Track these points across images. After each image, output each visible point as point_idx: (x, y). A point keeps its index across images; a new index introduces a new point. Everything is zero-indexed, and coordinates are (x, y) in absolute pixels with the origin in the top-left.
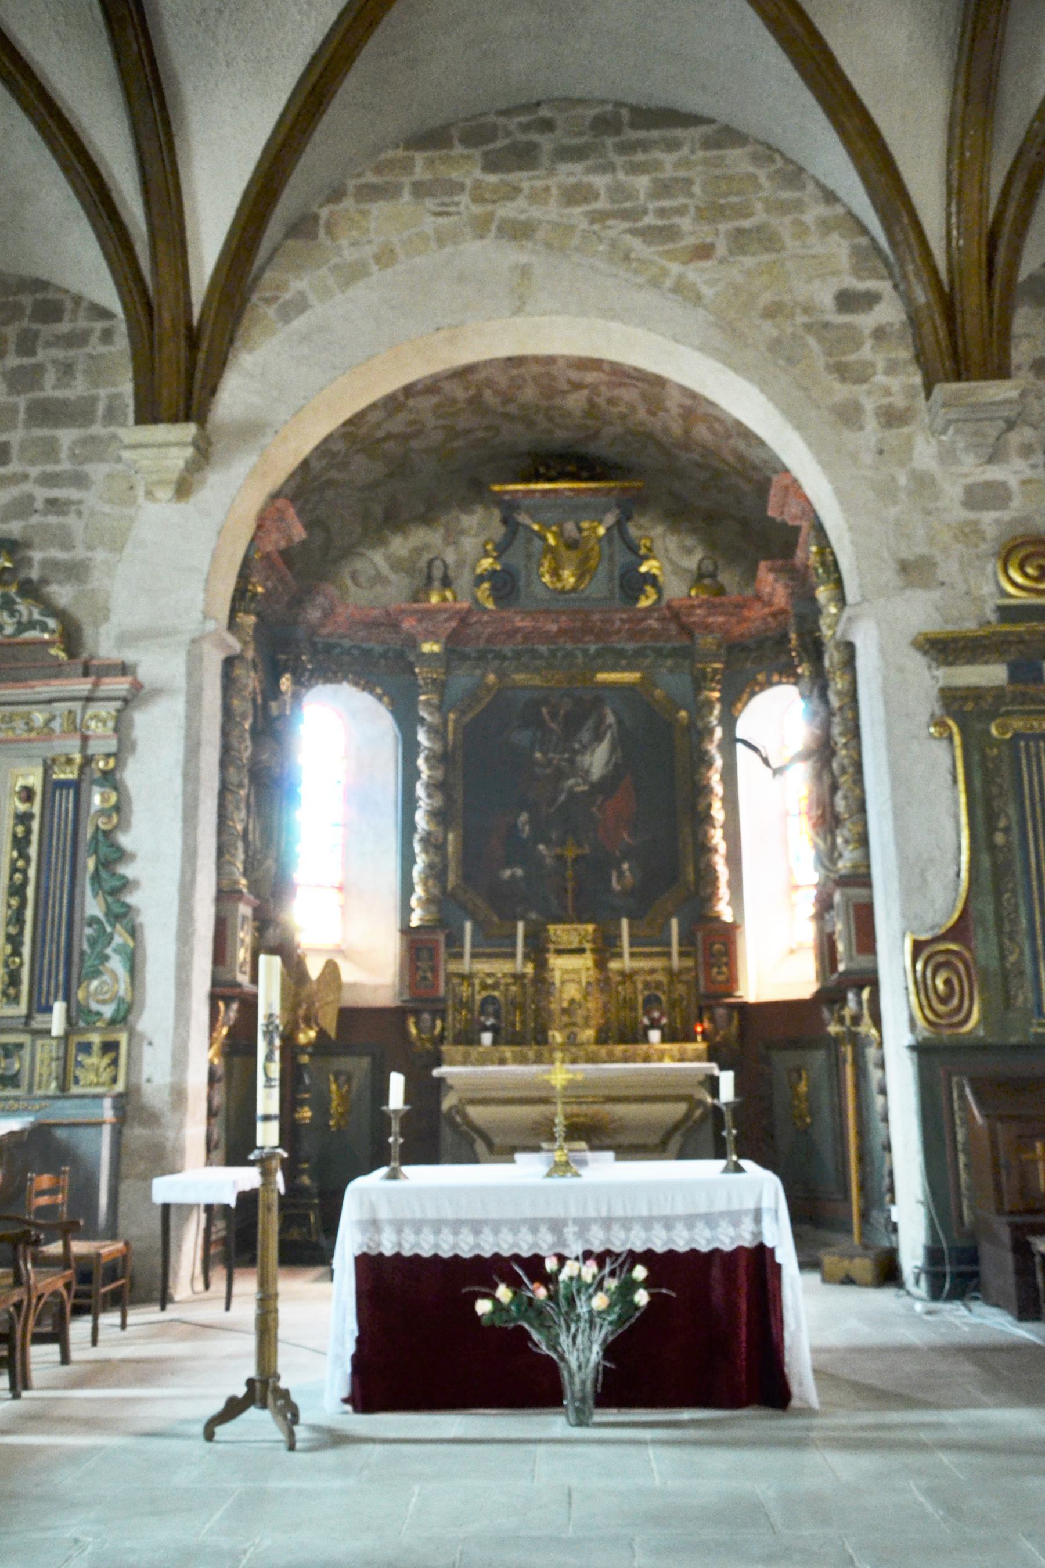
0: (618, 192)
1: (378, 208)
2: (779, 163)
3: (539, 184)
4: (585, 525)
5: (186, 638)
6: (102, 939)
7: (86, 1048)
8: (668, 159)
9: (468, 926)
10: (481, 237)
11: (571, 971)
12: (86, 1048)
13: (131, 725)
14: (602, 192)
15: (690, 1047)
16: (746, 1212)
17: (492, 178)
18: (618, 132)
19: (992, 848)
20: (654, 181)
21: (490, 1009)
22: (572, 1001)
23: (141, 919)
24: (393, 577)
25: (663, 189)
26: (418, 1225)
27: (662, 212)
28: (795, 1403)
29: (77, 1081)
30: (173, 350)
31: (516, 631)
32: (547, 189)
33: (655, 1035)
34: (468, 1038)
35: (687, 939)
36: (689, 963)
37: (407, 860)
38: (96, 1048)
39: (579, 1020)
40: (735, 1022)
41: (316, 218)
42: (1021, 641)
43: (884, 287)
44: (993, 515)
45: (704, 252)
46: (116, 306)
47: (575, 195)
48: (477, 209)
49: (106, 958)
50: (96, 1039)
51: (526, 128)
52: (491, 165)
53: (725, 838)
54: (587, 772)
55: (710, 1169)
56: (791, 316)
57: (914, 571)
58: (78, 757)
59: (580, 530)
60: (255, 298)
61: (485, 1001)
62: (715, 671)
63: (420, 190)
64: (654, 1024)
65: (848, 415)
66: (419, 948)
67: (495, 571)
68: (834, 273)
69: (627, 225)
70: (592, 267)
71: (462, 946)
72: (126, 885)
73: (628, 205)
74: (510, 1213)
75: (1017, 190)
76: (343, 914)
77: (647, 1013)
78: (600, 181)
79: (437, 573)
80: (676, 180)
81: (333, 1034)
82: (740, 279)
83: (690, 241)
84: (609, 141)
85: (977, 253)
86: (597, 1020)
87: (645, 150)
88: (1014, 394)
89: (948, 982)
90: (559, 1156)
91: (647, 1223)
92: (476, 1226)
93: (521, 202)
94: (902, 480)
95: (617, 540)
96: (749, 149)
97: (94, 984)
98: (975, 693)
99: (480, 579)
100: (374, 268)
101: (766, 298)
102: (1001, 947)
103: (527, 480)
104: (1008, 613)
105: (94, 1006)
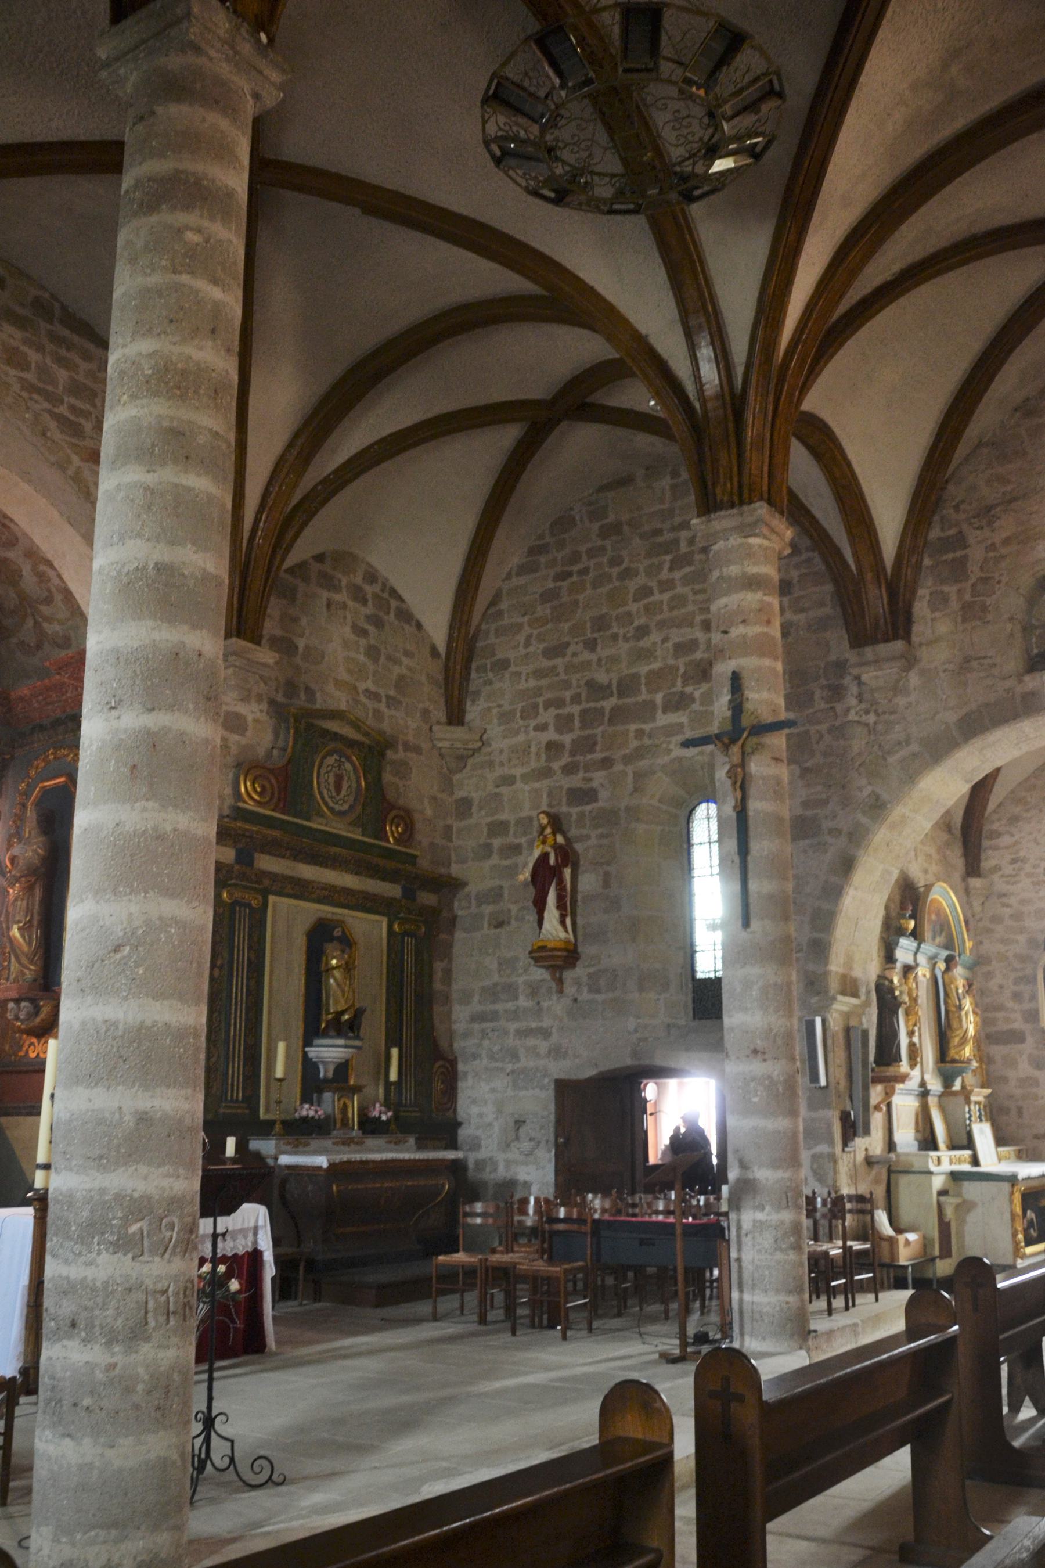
8: (84, 366)
14: (33, 365)
16: (248, 1229)
27: (72, 408)
42: (251, 837)
69: (46, 405)
73: (50, 388)
78: (34, 356)
87: (68, 349)
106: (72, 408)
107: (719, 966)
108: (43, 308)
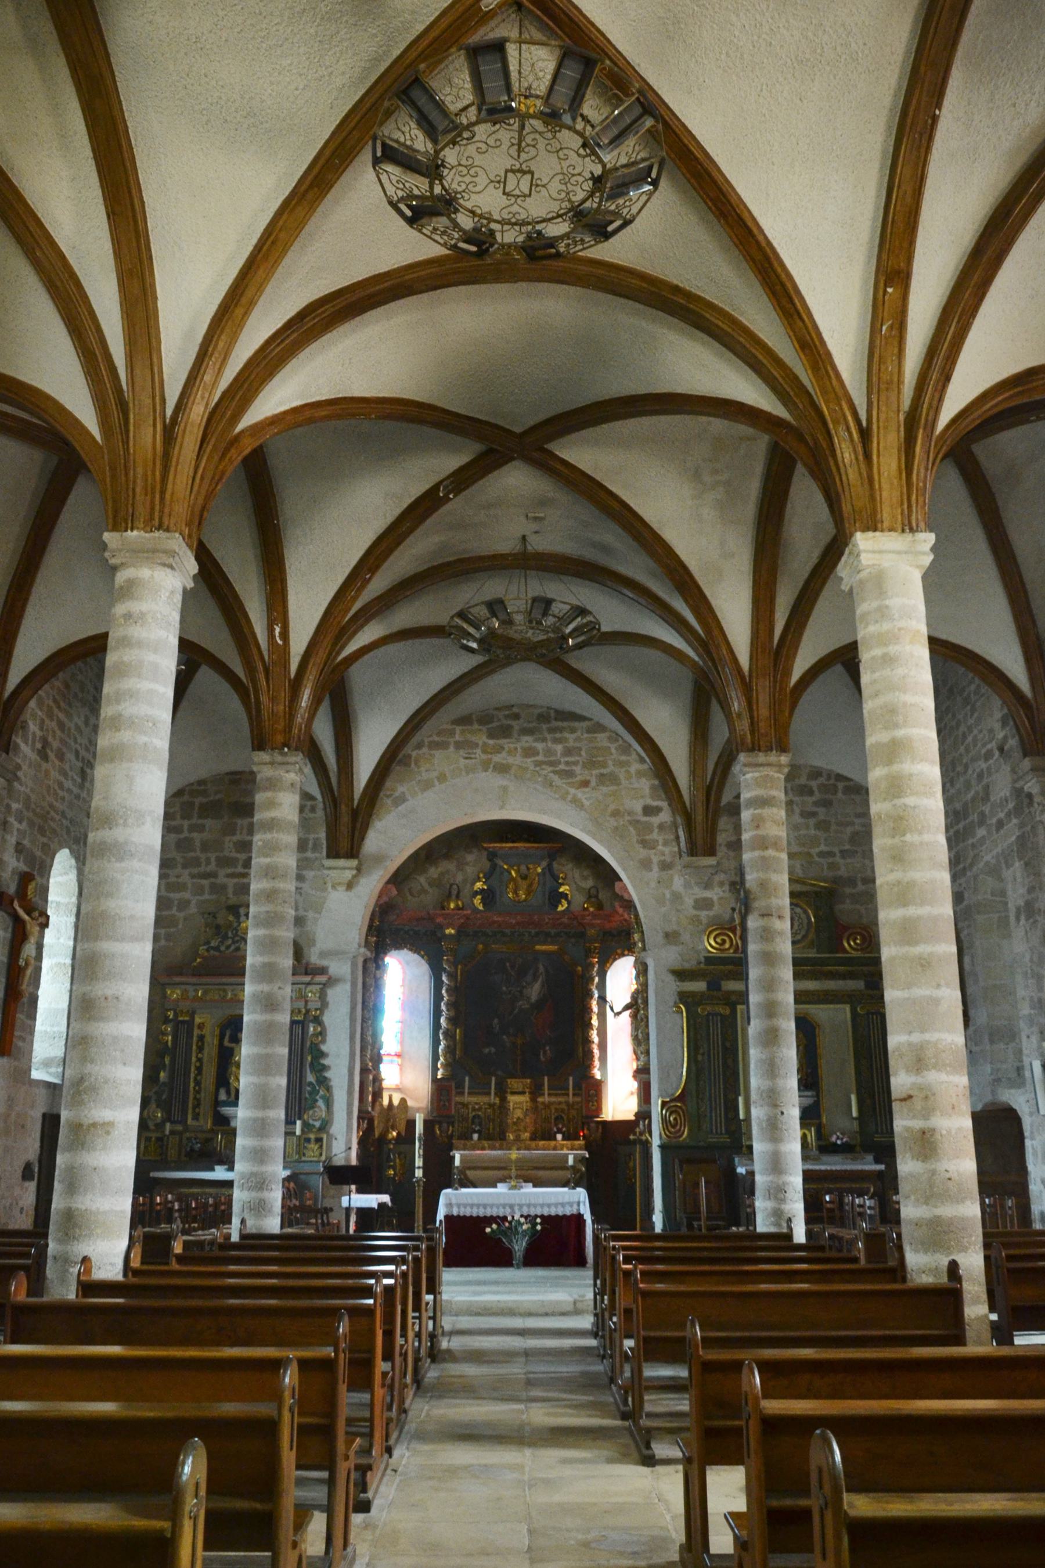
0: (549, 752)
1: (438, 754)
2: (621, 742)
3: (512, 746)
4: (531, 866)
5: (351, 955)
6: (314, 1092)
7: (308, 1140)
9: (467, 1078)
10: (486, 771)
11: (518, 1102)
12: (308, 1140)
13: (326, 995)
15: (577, 1143)
17: (491, 742)
18: (549, 722)
19: (696, 1061)
20: (565, 747)
21: (477, 1121)
22: (519, 1118)
23: (332, 1083)
24: (430, 890)
25: (568, 752)
26: (465, 1206)
27: (567, 763)
28: (770, 1556)
29: (304, 1155)
30: (345, 819)
31: (494, 922)
32: (516, 749)
33: (559, 1137)
34: (466, 1136)
35: (577, 1086)
36: (578, 1099)
37: (436, 1043)
38: (313, 1141)
39: (521, 1128)
40: (600, 1130)
41: (410, 756)
43: (664, 804)
44: (707, 913)
45: (585, 784)
46: (319, 797)
47: (529, 752)
48: (484, 757)
49: (317, 1101)
50: (312, 1136)
51: (507, 717)
52: (491, 735)
53: (598, 1035)
54: (529, 998)
55: (566, 1189)
56: (623, 815)
57: (671, 937)
58: (304, 1010)
59: (528, 869)
60: (381, 795)
61: (474, 1117)
62: (596, 948)
63: (458, 746)
64: (559, 1131)
65: (646, 864)
66: (441, 1089)
67: (483, 889)
68: (642, 797)
69: (551, 769)
70: (535, 789)
71: (464, 1088)
72: (325, 1068)
73: (552, 759)
74: (496, 1202)
75: (719, 773)
76: (401, 1069)
77: (556, 1125)
78: (540, 746)
79: (454, 892)
80: (574, 748)
81: (403, 1134)
82: (601, 798)
83: (579, 778)
84: (544, 726)
85: (701, 797)
86: (531, 1128)
88: (714, 863)
89: (675, 1119)
90: (513, 1183)
91: (542, 1206)
92: (485, 1206)
93: (504, 754)
94: (668, 896)
95: (548, 875)
96: (607, 734)
97: (311, 1112)
98: (692, 994)
99: (476, 893)
100: (436, 783)
101: (612, 807)
102: (698, 1103)
103: (501, 841)
104: (710, 960)
105: (311, 1122)
106: (567, 763)
107: (354, 1154)
108: (543, 718)
